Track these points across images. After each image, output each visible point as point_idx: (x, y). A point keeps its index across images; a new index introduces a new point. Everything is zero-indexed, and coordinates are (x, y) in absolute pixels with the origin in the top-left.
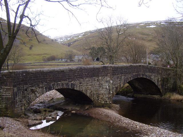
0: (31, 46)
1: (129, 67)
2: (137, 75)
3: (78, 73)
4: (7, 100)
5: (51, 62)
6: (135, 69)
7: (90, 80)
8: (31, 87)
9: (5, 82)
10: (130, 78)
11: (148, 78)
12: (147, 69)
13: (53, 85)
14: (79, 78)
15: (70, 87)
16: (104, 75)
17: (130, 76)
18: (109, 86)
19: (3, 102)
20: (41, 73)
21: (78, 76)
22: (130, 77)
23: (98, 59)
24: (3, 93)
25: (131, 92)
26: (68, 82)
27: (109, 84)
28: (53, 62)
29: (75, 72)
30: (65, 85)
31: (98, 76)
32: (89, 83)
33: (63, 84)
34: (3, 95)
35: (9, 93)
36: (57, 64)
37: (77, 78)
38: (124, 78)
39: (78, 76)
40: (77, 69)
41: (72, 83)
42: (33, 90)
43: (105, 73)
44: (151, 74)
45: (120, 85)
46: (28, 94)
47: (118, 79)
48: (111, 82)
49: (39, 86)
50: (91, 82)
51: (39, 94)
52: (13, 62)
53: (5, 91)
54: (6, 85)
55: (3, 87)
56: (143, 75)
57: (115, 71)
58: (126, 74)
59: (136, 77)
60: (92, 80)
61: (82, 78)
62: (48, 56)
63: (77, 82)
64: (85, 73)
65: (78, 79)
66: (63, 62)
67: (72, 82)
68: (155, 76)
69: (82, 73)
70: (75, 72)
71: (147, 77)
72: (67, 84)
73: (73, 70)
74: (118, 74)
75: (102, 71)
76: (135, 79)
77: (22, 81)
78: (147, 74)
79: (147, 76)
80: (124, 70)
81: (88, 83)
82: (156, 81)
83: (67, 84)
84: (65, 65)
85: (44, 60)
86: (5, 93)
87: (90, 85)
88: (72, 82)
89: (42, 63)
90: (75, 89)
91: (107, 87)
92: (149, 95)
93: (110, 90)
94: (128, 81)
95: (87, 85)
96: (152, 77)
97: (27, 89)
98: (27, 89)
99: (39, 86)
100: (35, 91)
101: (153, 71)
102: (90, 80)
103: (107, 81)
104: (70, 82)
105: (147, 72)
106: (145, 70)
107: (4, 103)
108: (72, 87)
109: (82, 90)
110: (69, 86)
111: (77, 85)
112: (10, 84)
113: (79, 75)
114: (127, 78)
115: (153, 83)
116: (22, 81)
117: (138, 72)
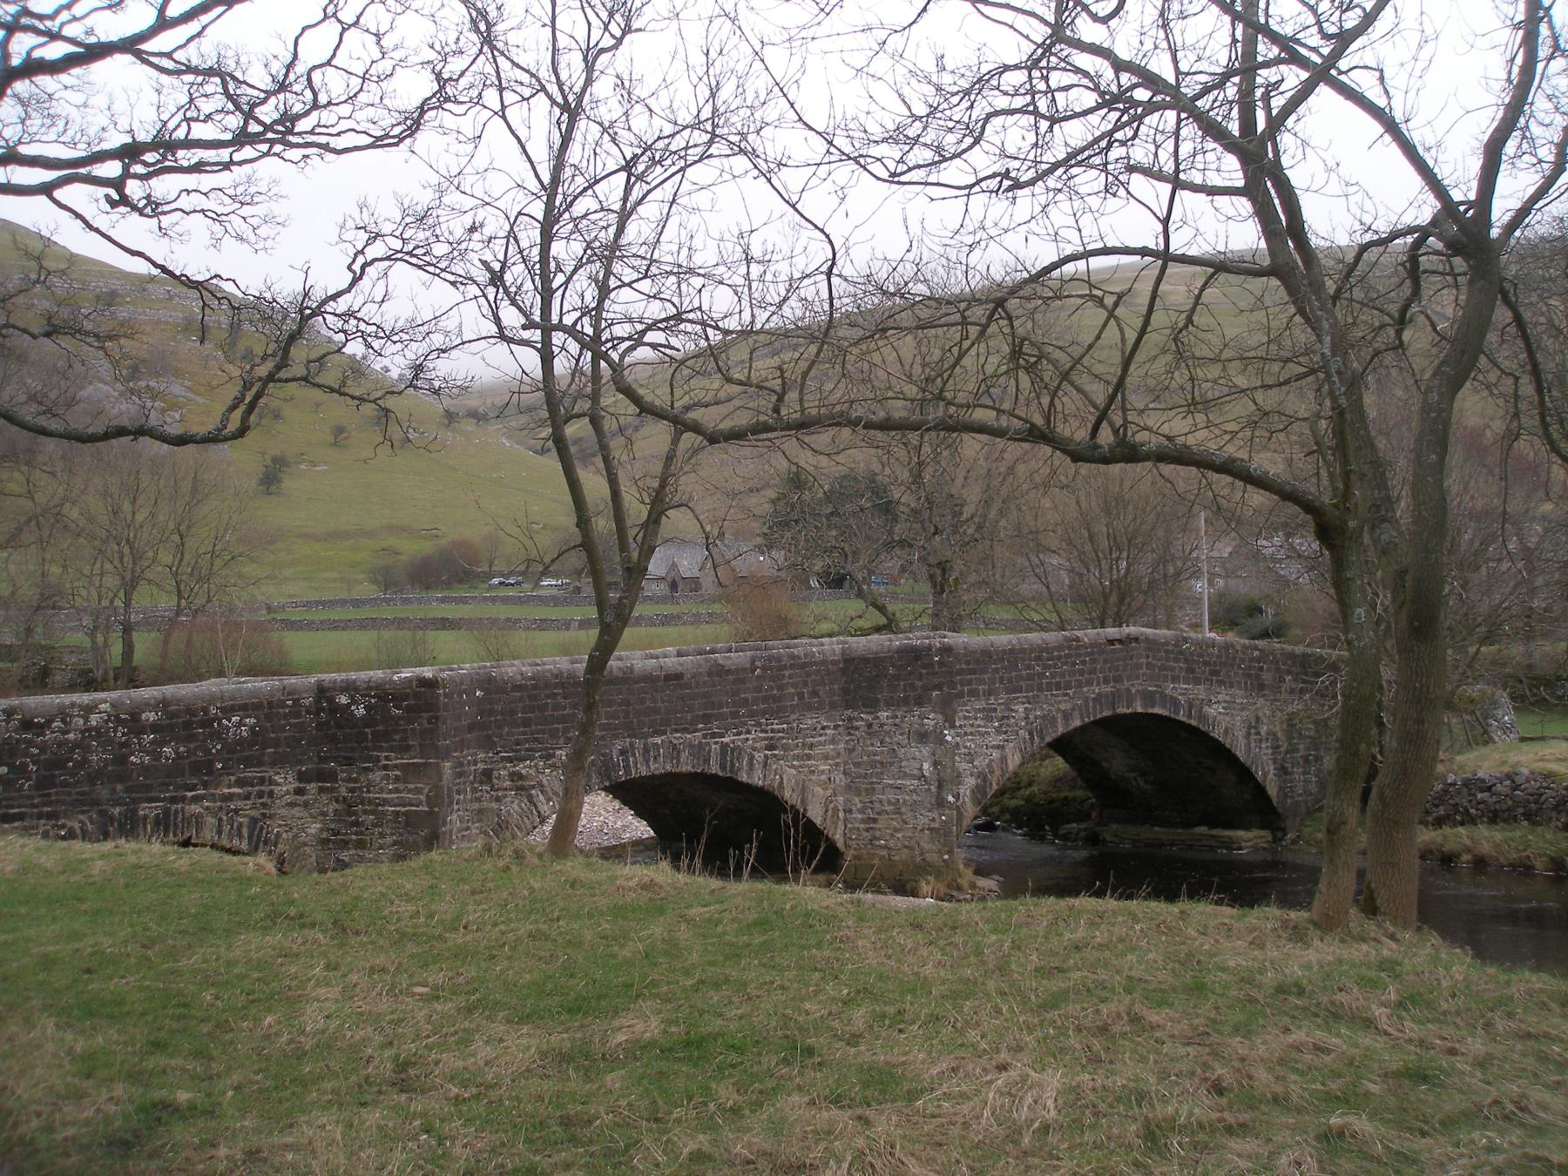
0: (275, 460)
1: (1060, 648)
2: (1114, 699)
3: (759, 689)
4: (407, 824)
5: (443, 600)
6: (1093, 661)
7: (823, 728)
8: (510, 760)
9: (396, 732)
10: (1067, 716)
11: (1182, 717)
12: (1176, 660)
13: (623, 752)
14: (764, 712)
15: (714, 769)
16: (906, 701)
17: (1063, 707)
18: (935, 764)
19: (382, 835)
20: (562, 685)
21: (756, 701)
22: (1069, 711)
23: (836, 582)
24: (382, 790)
25: (1082, 816)
26: (705, 736)
27: (939, 752)
28: (463, 600)
29: (743, 681)
30: (684, 755)
31: (872, 705)
32: (820, 743)
33: (675, 751)
34: (385, 802)
35: (418, 791)
36: (504, 612)
37: (752, 714)
38: (1027, 718)
39: (756, 701)
40: (753, 662)
41: (724, 746)
42: (521, 777)
43: (913, 687)
44: (1200, 691)
45: (1004, 759)
46: (498, 799)
47: (989, 719)
48: (949, 738)
49: (553, 756)
50: (833, 741)
51: (548, 800)
52: (166, 602)
53: (397, 779)
54: (405, 749)
55: (387, 758)
56: (1149, 698)
57: (973, 672)
58: (1040, 689)
59: (1107, 713)
60: (836, 727)
61: (778, 713)
62: (411, 549)
63: (753, 738)
64: (795, 685)
65: (759, 724)
66: (542, 600)
67: (726, 740)
68: (1229, 705)
69: (781, 688)
70: (743, 681)
71: (1177, 712)
72: (699, 751)
73: (729, 672)
74: (989, 693)
75: (897, 677)
76: (1095, 723)
77: (471, 728)
78: (1181, 690)
79: (1175, 703)
80: (1028, 667)
81: (811, 746)
82: (1240, 734)
83: (699, 751)
84: (567, 625)
85: (387, 579)
86: (397, 790)
87: (826, 757)
88: (726, 740)
89: (373, 602)
90: (743, 777)
91: (926, 766)
92: (1203, 829)
93: (940, 787)
94: (1054, 736)
95: (809, 757)
96: (1211, 711)
97: (491, 770)
98: (491, 770)
99: (553, 756)
100: (533, 787)
101: (1215, 673)
102: (823, 728)
103: (923, 737)
104: (714, 735)
105: (1175, 679)
106: (1162, 668)
107: (389, 840)
108: (723, 767)
109: (781, 783)
110: (707, 761)
111: (752, 758)
112: (421, 745)
113: (765, 700)
114: (1049, 720)
115: (1220, 753)
116: (471, 728)
117: (1118, 680)
